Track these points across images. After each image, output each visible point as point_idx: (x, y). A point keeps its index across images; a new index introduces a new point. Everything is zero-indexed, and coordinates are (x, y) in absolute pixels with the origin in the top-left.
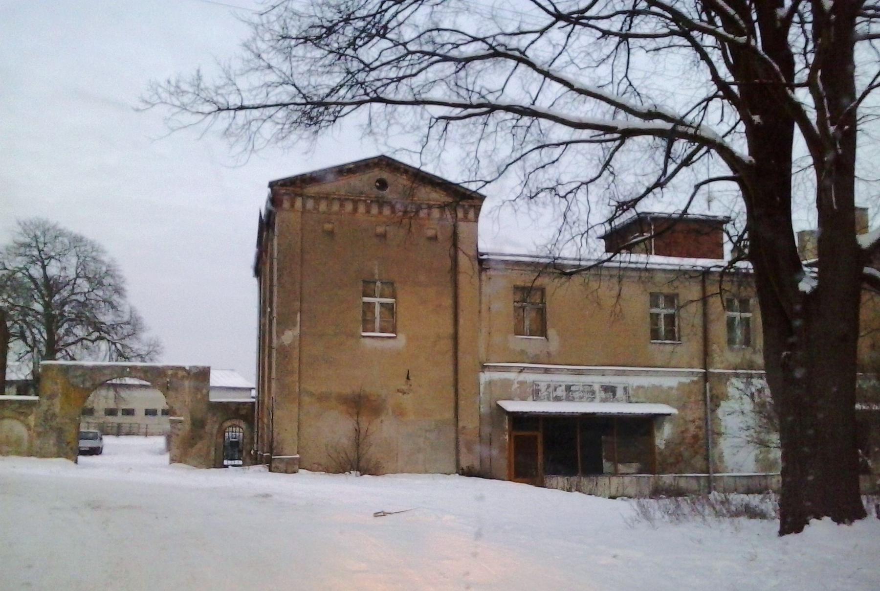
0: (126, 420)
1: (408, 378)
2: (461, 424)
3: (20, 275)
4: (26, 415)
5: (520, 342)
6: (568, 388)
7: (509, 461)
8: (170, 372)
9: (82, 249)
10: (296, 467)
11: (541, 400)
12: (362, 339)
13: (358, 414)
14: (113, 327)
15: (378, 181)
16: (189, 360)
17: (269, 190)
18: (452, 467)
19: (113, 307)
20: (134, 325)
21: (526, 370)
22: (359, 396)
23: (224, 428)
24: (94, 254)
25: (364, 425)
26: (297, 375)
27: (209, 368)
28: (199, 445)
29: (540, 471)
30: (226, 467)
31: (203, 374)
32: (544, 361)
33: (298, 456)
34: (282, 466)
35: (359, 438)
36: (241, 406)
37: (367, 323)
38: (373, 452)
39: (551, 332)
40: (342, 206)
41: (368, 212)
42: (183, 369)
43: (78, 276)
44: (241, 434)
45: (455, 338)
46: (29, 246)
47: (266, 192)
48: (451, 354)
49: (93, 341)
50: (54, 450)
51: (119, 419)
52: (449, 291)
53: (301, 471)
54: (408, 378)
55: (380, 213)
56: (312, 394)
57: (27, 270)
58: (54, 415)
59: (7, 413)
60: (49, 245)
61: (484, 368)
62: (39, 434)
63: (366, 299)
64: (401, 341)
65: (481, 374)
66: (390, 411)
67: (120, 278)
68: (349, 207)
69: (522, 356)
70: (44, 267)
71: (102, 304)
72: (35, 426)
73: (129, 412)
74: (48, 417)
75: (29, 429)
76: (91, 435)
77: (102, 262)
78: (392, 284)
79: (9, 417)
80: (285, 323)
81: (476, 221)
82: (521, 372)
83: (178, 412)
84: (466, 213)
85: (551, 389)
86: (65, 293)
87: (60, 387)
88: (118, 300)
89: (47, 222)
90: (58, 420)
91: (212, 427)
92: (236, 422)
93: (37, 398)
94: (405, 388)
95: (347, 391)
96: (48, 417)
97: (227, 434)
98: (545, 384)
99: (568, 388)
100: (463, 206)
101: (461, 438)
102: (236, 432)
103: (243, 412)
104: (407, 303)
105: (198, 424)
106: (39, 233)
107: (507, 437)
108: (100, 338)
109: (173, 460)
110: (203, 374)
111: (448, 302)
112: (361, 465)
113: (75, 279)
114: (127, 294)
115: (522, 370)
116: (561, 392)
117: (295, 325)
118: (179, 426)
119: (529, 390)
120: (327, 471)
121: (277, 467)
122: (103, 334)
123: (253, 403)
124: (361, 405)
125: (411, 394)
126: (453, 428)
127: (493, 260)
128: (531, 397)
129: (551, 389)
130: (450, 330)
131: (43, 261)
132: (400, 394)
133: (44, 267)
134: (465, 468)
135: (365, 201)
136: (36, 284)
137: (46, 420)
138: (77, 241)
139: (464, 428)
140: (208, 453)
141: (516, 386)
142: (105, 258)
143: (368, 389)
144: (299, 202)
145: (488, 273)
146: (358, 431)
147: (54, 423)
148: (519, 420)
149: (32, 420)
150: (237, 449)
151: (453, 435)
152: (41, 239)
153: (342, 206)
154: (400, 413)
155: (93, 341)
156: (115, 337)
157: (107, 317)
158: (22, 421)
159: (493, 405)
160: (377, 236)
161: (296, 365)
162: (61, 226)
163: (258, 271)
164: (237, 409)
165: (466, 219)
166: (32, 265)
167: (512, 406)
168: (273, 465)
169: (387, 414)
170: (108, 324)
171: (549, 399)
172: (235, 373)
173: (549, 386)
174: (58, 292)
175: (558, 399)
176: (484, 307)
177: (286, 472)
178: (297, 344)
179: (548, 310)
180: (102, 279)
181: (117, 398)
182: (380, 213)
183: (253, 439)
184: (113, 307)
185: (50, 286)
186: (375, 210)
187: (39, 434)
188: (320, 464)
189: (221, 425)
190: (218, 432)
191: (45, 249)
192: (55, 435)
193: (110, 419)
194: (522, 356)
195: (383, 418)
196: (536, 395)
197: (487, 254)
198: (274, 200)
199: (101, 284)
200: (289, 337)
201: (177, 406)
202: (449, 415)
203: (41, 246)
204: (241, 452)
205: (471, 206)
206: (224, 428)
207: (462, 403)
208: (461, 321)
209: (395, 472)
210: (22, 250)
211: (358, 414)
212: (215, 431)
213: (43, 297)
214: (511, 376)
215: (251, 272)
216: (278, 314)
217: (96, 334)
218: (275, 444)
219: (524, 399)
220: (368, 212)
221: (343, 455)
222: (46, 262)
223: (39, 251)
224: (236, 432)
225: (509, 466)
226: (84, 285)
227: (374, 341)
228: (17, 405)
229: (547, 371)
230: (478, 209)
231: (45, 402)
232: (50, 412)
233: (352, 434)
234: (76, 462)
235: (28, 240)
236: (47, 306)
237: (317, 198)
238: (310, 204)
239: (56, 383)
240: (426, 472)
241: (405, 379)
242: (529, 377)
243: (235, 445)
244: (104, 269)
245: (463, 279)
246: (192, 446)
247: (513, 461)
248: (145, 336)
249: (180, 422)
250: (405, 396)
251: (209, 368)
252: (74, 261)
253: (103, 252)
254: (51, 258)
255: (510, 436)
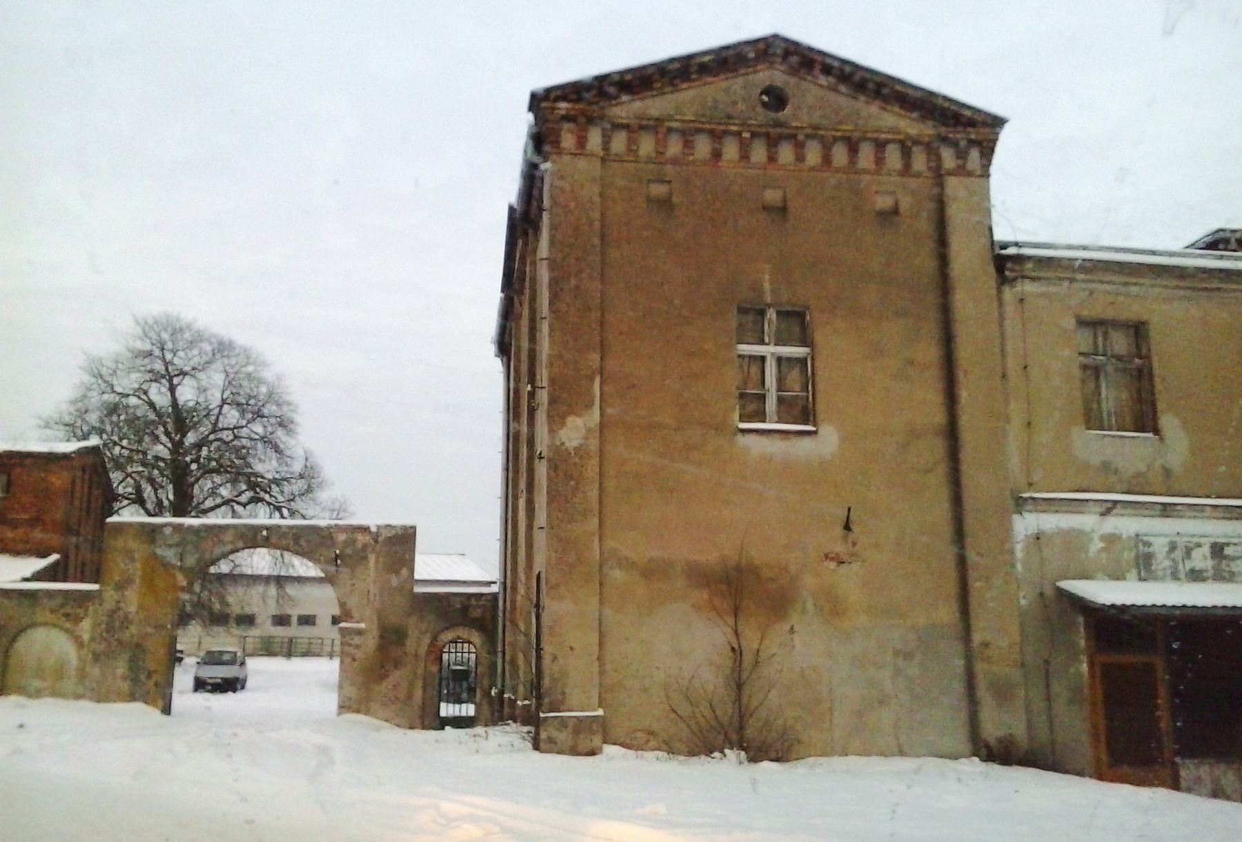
0: (306, 631)
1: (847, 527)
2: (977, 638)
3: (133, 401)
4: (77, 620)
5: (1094, 445)
6: (1218, 550)
7: (1094, 726)
8: (342, 537)
9: (233, 361)
10: (597, 740)
11: (1156, 579)
12: (740, 437)
13: (736, 611)
14: (276, 482)
15: (767, 91)
16: (373, 513)
17: (530, 117)
18: (960, 739)
19: (277, 450)
20: (310, 478)
21: (1118, 506)
22: (739, 569)
23: (440, 644)
24: (250, 368)
25: (750, 640)
26: (596, 520)
27: (414, 528)
28: (396, 675)
29: (1169, 745)
30: (442, 723)
31: (401, 543)
32: (1157, 489)
33: (600, 712)
34: (563, 737)
35: (740, 672)
36: (473, 602)
37: (753, 406)
38: (772, 703)
39: (1168, 422)
40: (688, 145)
41: (745, 156)
42: (365, 529)
43: (224, 402)
44: (473, 656)
45: (952, 432)
46: (150, 354)
47: (524, 121)
48: (942, 470)
49: (244, 505)
50: (125, 686)
51: (294, 631)
52: (930, 329)
53: (609, 749)
54: (847, 527)
55: (772, 159)
56: (628, 565)
57: (146, 393)
58: (126, 621)
59: (42, 615)
60: (181, 354)
61: (1020, 504)
62: (96, 657)
63: (745, 349)
64: (827, 441)
65: (1016, 517)
66: (810, 605)
67: (289, 404)
68: (703, 147)
69: (1106, 475)
70: (172, 389)
71: (260, 445)
72: (93, 639)
73: (307, 620)
74: (115, 622)
75: (80, 644)
76: (226, 657)
77: (260, 381)
78: (800, 316)
79: (46, 624)
80: (566, 401)
81: (986, 175)
82: (1105, 514)
83: (355, 613)
84: (962, 155)
85: (1178, 554)
86: (204, 429)
87: (138, 565)
88: (284, 438)
89: (178, 319)
90: (133, 629)
91: (417, 642)
92: (462, 632)
93: (95, 587)
94: (840, 548)
95: (709, 557)
96: (115, 622)
97: (445, 656)
98: (1165, 541)
99: (1218, 550)
100: (955, 144)
101: (980, 667)
102: (464, 652)
103: (476, 613)
104: (838, 349)
105: (391, 637)
106: (165, 336)
107: (1085, 667)
108: (256, 500)
109: (344, 707)
110: (401, 543)
111: (930, 352)
112: (750, 733)
113: (221, 407)
114: (299, 430)
115: (1109, 509)
116: (1201, 559)
117: (589, 406)
118: (357, 640)
119: (1128, 556)
120: (670, 748)
121: (551, 740)
122: (262, 494)
123: (494, 596)
124: (742, 590)
125: (856, 566)
126: (959, 648)
127: (1029, 258)
128: (1134, 572)
129: (1178, 554)
130: (939, 417)
131: (171, 377)
132: (832, 565)
133: (172, 389)
134: (992, 742)
135: (739, 134)
136: (159, 415)
137: (110, 629)
138: (223, 348)
139: (986, 645)
140: (410, 696)
141: (1097, 545)
142: (268, 375)
143: (757, 554)
144: (595, 139)
145: (1018, 288)
146: (737, 652)
147: (126, 636)
148: (1112, 627)
149: (85, 628)
150: (465, 685)
151: (960, 663)
152: (169, 345)
153: (688, 145)
154: (832, 608)
155: (244, 505)
156: (281, 499)
157: (266, 466)
158: (67, 631)
159: (1049, 592)
160: (766, 208)
161: (594, 493)
162: (200, 324)
163: (504, 347)
164: (465, 609)
165: (962, 171)
166: (154, 385)
167: (1105, 592)
168: (543, 735)
169: (804, 611)
170: (270, 476)
171: (1175, 577)
172: (461, 551)
173: (1173, 547)
174: (195, 426)
175: (1196, 576)
176: (1012, 365)
177: (574, 751)
178: (594, 444)
179: (1157, 371)
180: (259, 406)
181: (282, 598)
182: (772, 159)
183: (494, 664)
184: (277, 450)
185: (180, 419)
186: (759, 153)
187: (96, 657)
188: (651, 733)
189: (435, 638)
190: (428, 653)
191: (176, 361)
192: (126, 657)
193: (280, 631)
194: (1106, 475)
195: (794, 619)
196: (1144, 566)
197: (1016, 244)
198: (541, 140)
199: (259, 415)
200: (576, 431)
201: (352, 603)
202: (947, 613)
203: (169, 356)
204: (471, 691)
205: (972, 143)
206: (440, 644)
207: (976, 585)
208: (964, 395)
209: (827, 751)
210: (139, 362)
211: (736, 611)
212: (423, 650)
213: (167, 434)
214: (1086, 521)
215: (492, 349)
216: (552, 381)
217: (249, 494)
218: (546, 682)
219: (1118, 576)
220: (745, 156)
221: (708, 713)
222: (176, 381)
223: (166, 364)
224: (464, 652)
225: (1095, 737)
226: (231, 416)
227: (766, 444)
228: (59, 600)
229: (1166, 511)
230: (987, 150)
231: (111, 596)
232: (121, 613)
233: (727, 661)
234: (167, 710)
235: (148, 347)
236: (177, 447)
237: (633, 129)
238: (619, 143)
239: (133, 560)
240: (902, 753)
241: (839, 531)
242: (1126, 525)
243: (461, 676)
244: (264, 389)
245: (962, 301)
246: (383, 677)
247: (1102, 723)
248: (324, 495)
249: (360, 632)
250: (843, 570)
251: (414, 528)
252: (218, 379)
253: (264, 364)
254: (183, 373)
255: (1091, 665)
